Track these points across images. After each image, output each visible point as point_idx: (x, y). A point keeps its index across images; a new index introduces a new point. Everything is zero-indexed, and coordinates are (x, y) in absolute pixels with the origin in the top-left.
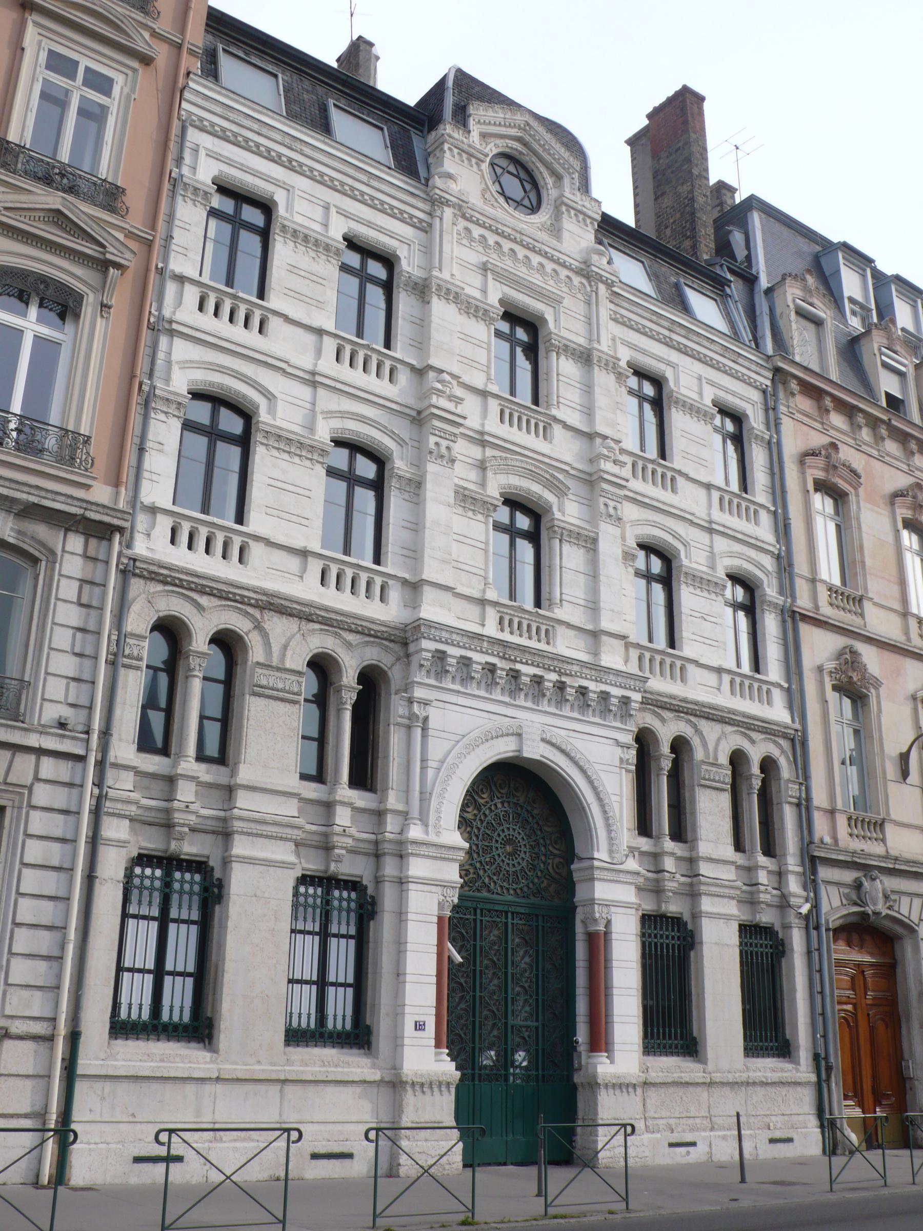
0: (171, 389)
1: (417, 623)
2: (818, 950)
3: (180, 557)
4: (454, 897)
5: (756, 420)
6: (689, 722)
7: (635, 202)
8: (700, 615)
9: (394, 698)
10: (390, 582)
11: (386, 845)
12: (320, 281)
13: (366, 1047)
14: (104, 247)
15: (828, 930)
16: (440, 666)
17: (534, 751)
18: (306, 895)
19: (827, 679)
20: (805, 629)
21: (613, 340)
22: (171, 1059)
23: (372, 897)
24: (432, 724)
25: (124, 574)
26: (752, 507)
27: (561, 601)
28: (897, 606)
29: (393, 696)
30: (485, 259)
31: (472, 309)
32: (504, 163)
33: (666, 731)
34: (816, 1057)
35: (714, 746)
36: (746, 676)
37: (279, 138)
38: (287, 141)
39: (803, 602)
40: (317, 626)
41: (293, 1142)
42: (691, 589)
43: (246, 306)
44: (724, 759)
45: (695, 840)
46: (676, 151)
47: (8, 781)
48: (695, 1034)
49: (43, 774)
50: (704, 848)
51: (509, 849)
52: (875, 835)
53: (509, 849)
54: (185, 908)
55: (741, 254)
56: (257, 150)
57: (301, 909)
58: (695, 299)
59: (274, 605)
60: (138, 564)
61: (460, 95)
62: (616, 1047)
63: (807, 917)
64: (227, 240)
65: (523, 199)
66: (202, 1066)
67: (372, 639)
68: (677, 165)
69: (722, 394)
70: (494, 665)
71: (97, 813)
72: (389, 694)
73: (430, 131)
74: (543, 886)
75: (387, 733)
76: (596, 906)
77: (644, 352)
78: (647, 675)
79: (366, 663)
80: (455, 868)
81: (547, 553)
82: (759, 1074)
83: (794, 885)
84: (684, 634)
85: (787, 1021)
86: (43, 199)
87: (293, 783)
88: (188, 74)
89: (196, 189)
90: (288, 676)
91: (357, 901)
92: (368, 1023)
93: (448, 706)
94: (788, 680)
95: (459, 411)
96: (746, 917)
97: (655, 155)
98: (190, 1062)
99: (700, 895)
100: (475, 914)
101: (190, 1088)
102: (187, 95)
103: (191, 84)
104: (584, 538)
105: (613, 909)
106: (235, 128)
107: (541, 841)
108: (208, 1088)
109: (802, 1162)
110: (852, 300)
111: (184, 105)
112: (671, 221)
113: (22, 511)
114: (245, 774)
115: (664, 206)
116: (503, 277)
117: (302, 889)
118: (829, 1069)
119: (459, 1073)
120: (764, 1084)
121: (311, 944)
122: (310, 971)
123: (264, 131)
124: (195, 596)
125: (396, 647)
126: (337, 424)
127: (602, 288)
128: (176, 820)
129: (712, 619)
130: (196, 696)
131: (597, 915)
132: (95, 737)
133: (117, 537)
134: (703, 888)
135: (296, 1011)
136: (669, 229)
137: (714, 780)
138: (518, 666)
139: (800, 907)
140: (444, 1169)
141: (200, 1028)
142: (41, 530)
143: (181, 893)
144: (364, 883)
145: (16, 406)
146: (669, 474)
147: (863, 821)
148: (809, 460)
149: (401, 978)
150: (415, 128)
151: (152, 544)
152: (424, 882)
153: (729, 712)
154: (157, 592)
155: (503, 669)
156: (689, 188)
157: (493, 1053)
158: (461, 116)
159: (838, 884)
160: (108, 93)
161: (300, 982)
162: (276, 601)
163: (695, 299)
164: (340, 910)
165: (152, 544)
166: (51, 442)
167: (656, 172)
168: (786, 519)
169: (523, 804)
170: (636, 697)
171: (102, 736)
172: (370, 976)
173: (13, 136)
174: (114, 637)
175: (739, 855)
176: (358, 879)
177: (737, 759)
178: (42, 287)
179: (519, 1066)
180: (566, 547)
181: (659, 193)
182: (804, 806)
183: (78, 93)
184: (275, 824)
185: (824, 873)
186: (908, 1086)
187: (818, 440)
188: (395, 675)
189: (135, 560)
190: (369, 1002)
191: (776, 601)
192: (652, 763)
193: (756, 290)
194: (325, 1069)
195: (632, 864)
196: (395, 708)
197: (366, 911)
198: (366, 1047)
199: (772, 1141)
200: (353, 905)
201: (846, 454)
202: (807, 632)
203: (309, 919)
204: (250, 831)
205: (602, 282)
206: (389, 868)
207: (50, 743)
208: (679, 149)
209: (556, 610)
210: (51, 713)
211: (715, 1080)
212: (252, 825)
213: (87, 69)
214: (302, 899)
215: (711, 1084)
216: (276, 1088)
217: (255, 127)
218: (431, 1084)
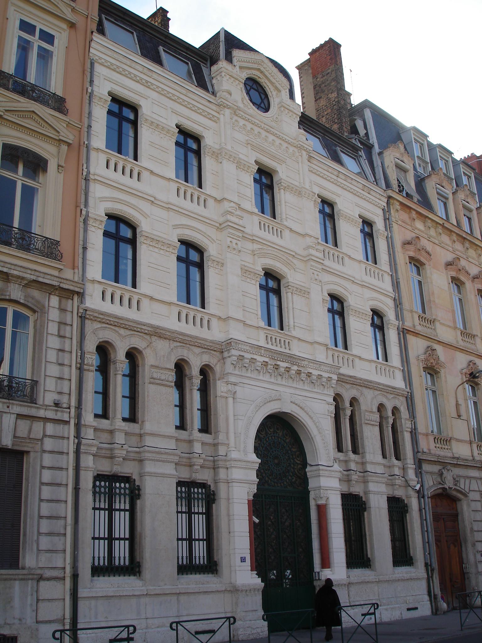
0: (97, 213)
1: (230, 341)
2: (424, 509)
3: (107, 307)
4: (254, 489)
5: (379, 225)
6: (357, 390)
7: (302, 101)
8: (359, 332)
9: (219, 383)
10: (212, 319)
11: (220, 463)
12: (166, 151)
13: (215, 572)
14: (58, 132)
15: (428, 498)
16: (265, 369)
17: (288, 408)
18: (100, 487)
19: (421, 364)
20: (410, 337)
21: (311, 182)
22: (123, 586)
23: (213, 491)
24: (238, 395)
25: (82, 318)
26: (381, 273)
27: (294, 326)
28: (451, 324)
29: (217, 381)
30: (247, 138)
31: (240, 165)
32: (250, 83)
33: (347, 394)
34: (426, 565)
35: (369, 402)
36: (380, 363)
37: (141, 69)
38: (146, 71)
39: (408, 324)
40: (179, 344)
41: (232, 624)
42: (354, 318)
43: (138, 169)
44: (375, 409)
45: (364, 453)
46: (327, 74)
47: (31, 437)
48: (369, 556)
49: (48, 433)
50: (369, 457)
51: (276, 461)
52: (440, 446)
53: (276, 461)
54: (122, 503)
55: (362, 132)
56: (128, 76)
57: (97, 495)
58: (345, 158)
59: (157, 333)
60: (88, 312)
61: (228, 44)
62: (335, 565)
63: (418, 492)
64: (116, 127)
65: (260, 104)
66: (138, 588)
67: (206, 350)
68: (328, 82)
69: (363, 211)
70: (267, 362)
71: (77, 452)
72: (215, 380)
73: (212, 64)
74: (293, 480)
75: (215, 401)
76: (322, 491)
77: (325, 189)
78: (341, 365)
79: (203, 364)
80: (254, 473)
81: (286, 300)
82: (401, 575)
83: (411, 474)
84: (353, 342)
85: (411, 547)
86: (25, 105)
87: (172, 431)
88: (92, 32)
89: (101, 98)
90: (167, 372)
91: (129, 489)
92: (215, 560)
93: (246, 385)
94: (403, 366)
95: (241, 222)
96: (345, 489)
97: (314, 76)
98: (132, 587)
99: (368, 482)
100: (262, 498)
101: (134, 601)
102: (93, 44)
103: (94, 38)
104: (303, 292)
105: (329, 492)
106: (118, 64)
107: (291, 457)
108: (143, 600)
109: (424, 619)
110: (418, 157)
111: (91, 50)
112: (326, 113)
113: (26, 284)
114: (148, 427)
115: (321, 105)
116: (254, 148)
117: (98, 483)
118: (432, 570)
119: (263, 584)
120: (403, 580)
121: (104, 515)
122: (103, 533)
123: (133, 65)
124: (117, 329)
125: (218, 354)
126: (179, 231)
127: (304, 153)
128: (116, 455)
129: (365, 334)
130: (119, 386)
131: (322, 495)
132: (73, 410)
133: (76, 298)
134: (369, 478)
135: (96, 555)
136: (324, 118)
137: (371, 421)
138: (279, 363)
139: (415, 486)
140: (260, 635)
141: (211, 567)
142: (36, 294)
143: (120, 494)
144: (134, 477)
145: (16, 224)
146: (341, 255)
147: (441, 439)
148: (407, 246)
149: (232, 534)
150: (203, 63)
151: (94, 301)
152: (241, 482)
153: (376, 384)
154: (98, 328)
155: (271, 365)
156: (336, 95)
157: (275, 572)
158: (229, 58)
159: (431, 473)
160: (52, 44)
161: (99, 539)
162: (158, 331)
163: (345, 158)
164: (120, 494)
165: (94, 301)
166: (39, 245)
167: (315, 86)
168: (397, 278)
169: (280, 437)
170: (335, 377)
171: (77, 409)
172: (215, 534)
173: (5, 69)
174: (79, 354)
175: (340, 454)
176: (205, 482)
177: (381, 408)
178: (26, 155)
179: (288, 579)
180: (295, 297)
181: (317, 98)
182: (414, 433)
183: (36, 42)
184: (166, 453)
185: (426, 467)
186: (466, 577)
187: (409, 236)
188: (218, 369)
189: (86, 310)
190: (215, 548)
191: (395, 323)
192: (341, 412)
193: (373, 153)
194: (198, 586)
195: (336, 467)
196: (220, 388)
197: (210, 498)
198: (215, 572)
199: (409, 609)
200: (127, 492)
201: (424, 242)
202: (411, 339)
203: (102, 500)
204: (153, 458)
205: (305, 150)
206: (222, 474)
207: (50, 414)
208: (329, 73)
209: (292, 332)
210: (50, 398)
211: (381, 579)
212: (154, 455)
213: (41, 30)
214: (97, 489)
215: (379, 582)
216: (175, 598)
217: (128, 62)
218: (250, 590)
